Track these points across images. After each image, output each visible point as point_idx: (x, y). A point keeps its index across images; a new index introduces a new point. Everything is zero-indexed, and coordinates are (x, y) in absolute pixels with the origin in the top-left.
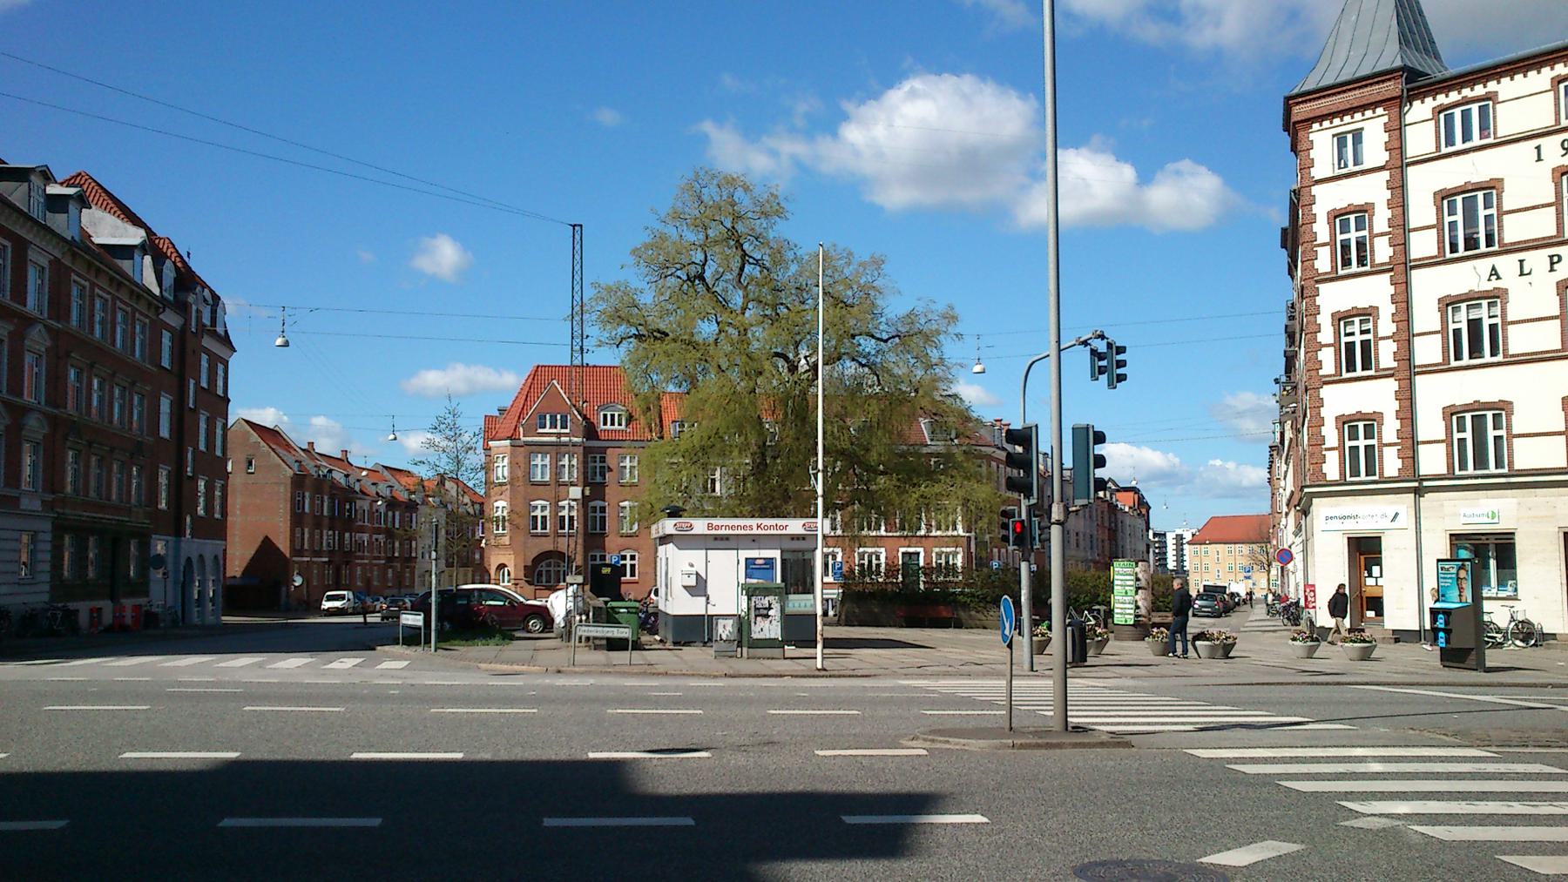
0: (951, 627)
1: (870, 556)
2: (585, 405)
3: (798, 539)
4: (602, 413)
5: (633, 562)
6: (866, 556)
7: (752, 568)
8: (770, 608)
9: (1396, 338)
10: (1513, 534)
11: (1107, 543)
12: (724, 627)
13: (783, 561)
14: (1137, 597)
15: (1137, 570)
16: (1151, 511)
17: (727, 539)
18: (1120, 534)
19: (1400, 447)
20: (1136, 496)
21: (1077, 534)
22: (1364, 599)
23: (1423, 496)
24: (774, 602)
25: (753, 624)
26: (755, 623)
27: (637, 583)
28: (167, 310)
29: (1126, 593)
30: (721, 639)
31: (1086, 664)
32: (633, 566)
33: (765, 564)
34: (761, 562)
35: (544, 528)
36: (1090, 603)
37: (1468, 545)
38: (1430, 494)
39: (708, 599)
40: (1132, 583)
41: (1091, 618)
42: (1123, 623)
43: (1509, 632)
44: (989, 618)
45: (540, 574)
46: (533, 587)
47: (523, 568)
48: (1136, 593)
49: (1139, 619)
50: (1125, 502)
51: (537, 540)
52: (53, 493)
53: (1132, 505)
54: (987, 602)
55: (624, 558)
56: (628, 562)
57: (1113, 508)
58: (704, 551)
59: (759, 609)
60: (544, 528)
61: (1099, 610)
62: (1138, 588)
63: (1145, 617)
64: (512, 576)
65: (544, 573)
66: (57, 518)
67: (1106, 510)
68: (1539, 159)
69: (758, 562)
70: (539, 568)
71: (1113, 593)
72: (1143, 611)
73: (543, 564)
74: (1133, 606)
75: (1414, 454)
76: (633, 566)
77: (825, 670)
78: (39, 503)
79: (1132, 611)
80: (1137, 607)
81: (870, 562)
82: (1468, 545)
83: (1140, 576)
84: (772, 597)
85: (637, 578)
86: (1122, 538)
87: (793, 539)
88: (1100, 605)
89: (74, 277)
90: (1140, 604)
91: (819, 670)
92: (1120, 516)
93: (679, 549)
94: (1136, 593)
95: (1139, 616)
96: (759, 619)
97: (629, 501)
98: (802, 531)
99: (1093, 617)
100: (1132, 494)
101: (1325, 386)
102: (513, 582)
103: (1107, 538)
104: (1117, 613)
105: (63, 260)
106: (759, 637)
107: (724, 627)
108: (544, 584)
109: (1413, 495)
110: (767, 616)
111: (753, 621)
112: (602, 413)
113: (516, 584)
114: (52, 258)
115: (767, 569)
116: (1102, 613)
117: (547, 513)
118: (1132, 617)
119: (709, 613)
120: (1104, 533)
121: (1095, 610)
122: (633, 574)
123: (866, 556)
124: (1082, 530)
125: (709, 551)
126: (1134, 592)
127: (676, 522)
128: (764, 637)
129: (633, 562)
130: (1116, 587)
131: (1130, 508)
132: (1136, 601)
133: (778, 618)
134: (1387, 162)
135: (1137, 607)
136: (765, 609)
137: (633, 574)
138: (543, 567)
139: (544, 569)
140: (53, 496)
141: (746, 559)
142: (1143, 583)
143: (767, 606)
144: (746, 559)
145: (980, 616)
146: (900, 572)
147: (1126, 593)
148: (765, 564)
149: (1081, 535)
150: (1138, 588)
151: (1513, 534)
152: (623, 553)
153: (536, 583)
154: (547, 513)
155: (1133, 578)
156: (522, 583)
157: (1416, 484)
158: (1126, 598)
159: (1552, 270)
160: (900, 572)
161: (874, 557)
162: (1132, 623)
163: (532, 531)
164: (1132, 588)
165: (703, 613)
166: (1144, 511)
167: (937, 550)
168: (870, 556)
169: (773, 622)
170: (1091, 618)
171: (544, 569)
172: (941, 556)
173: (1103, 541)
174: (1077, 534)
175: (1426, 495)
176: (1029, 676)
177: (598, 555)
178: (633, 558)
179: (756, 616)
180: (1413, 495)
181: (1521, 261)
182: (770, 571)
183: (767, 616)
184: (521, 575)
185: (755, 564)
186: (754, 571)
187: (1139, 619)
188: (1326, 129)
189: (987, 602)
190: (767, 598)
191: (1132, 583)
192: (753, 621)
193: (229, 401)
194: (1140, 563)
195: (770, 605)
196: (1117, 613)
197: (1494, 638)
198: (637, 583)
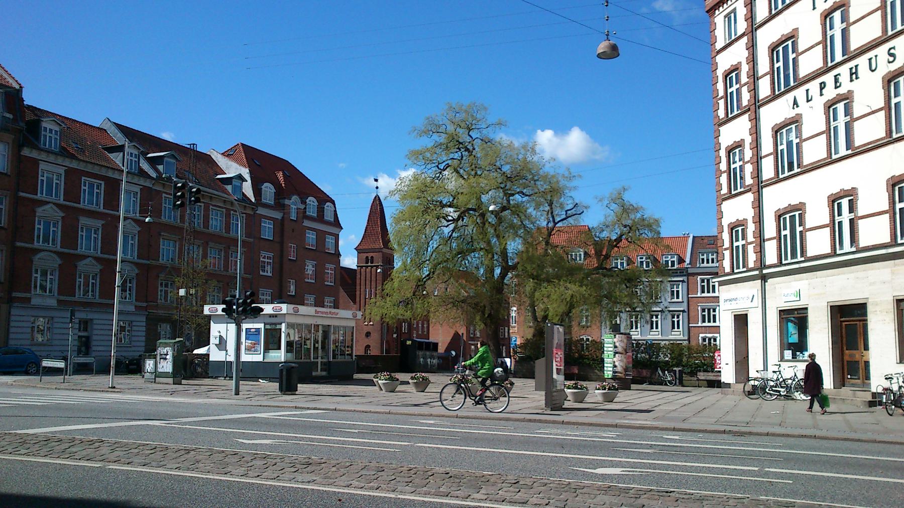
0: (715, 387)
1: (710, 339)
3: (273, 317)
6: (707, 340)
7: (249, 334)
8: (167, 354)
9: (752, 162)
10: (806, 309)
12: (149, 364)
13: (266, 330)
14: (615, 359)
15: (615, 340)
17: (276, 316)
19: (754, 245)
22: (845, 363)
23: (767, 282)
24: (169, 351)
25: (158, 363)
26: (160, 363)
28: (259, 207)
30: (148, 372)
31: (297, 393)
33: (255, 332)
34: (254, 330)
37: (792, 319)
38: (770, 279)
39: (227, 351)
40: (611, 349)
43: (793, 386)
49: (616, 374)
52: (147, 302)
58: (226, 324)
59: (162, 355)
62: (616, 353)
66: (148, 315)
68: (814, 8)
69: (252, 330)
72: (619, 369)
74: (612, 365)
75: (761, 249)
77: (114, 388)
78: (134, 307)
79: (611, 369)
80: (615, 366)
81: (710, 343)
82: (792, 319)
83: (617, 344)
84: (168, 348)
87: (270, 317)
89: (164, 195)
91: (109, 387)
93: (214, 323)
94: (614, 355)
95: (616, 372)
96: (162, 360)
98: (272, 312)
101: (724, 203)
105: (154, 188)
106: (161, 371)
107: (149, 364)
109: (760, 281)
110: (165, 359)
111: (159, 361)
114: (142, 187)
115: (257, 334)
118: (611, 373)
119: (227, 360)
123: (707, 340)
125: (228, 324)
127: (209, 307)
128: (163, 371)
132: (614, 362)
133: (171, 360)
134: (746, 29)
135: (615, 366)
136: (165, 355)
140: (147, 304)
141: (246, 329)
142: (620, 349)
143: (166, 353)
144: (246, 329)
146: (585, 348)
148: (255, 332)
150: (616, 353)
151: (806, 309)
155: (612, 345)
157: (765, 271)
159: (821, 95)
160: (585, 348)
161: (712, 340)
164: (611, 353)
165: (224, 360)
167: (701, 335)
168: (710, 339)
169: (169, 362)
172: (705, 339)
175: (768, 280)
176: (107, 391)
179: (160, 359)
180: (760, 281)
181: (807, 91)
182: (258, 335)
183: (165, 359)
185: (250, 332)
186: (250, 336)
187: (616, 374)
188: (718, 15)
190: (166, 349)
191: (611, 349)
192: (159, 361)
193: (339, 255)
195: (167, 352)
197: (779, 391)
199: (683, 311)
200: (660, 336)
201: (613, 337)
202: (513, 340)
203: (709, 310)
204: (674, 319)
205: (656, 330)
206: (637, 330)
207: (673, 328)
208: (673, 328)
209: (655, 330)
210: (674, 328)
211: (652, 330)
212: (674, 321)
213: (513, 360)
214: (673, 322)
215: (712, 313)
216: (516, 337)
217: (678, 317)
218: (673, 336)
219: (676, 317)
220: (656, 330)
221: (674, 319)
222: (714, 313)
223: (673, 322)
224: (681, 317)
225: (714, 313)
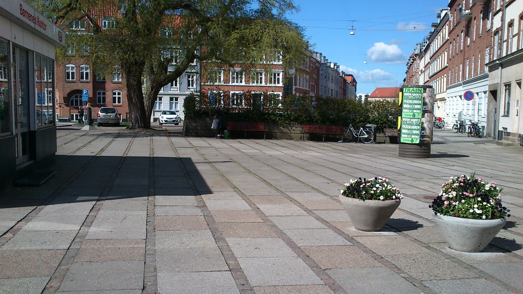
2: (95, 17)
4: (103, 21)
5: (119, 96)
11: (342, 95)
14: (424, 120)
15: (425, 95)
16: (357, 84)
18: (347, 92)
20: (352, 78)
21: (332, 90)
27: (122, 106)
29: (414, 115)
32: (119, 98)
35: (73, 78)
36: (363, 121)
40: (419, 107)
41: (365, 133)
42: (410, 142)
44: (292, 131)
45: (72, 101)
46: (69, 108)
47: (63, 99)
48: (423, 116)
49: (424, 139)
50: (349, 79)
51: (69, 84)
53: (351, 81)
54: (291, 120)
55: (115, 94)
56: (117, 96)
57: (345, 81)
60: (73, 78)
61: (370, 127)
63: (429, 137)
64: (58, 102)
65: (74, 101)
67: (343, 81)
70: (72, 98)
71: (401, 116)
73: (74, 96)
76: (119, 98)
79: (418, 132)
80: (423, 129)
85: (121, 104)
86: (348, 93)
88: (370, 123)
90: (425, 125)
92: (347, 85)
94: (423, 116)
97: (141, 74)
99: (367, 132)
100: (351, 77)
102: (58, 105)
103: (342, 93)
104: (404, 134)
108: (74, 106)
112: (103, 21)
113: (60, 106)
116: (373, 129)
117: (74, 71)
118: (418, 137)
120: (341, 90)
121: (368, 127)
122: (119, 102)
124: (333, 89)
125: (149, 156)
126: (421, 114)
129: (119, 96)
130: (404, 111)
131: (350, 82)
132: (423, 123)
135: (423, 129)
137: (119, 102)
138: (73, 98)
139: (74, 99)
145: (285, 130)
147: (414, 115)
149: (333, 91)
152: (114, 92)
153: (70, 106)
154: (74, 71)
156: (63, 106)
158: (414, 120)
162: (418, 142)
163: (81, 80)
166: (355, 84)
170: (365, 133)
171: (74, 99)
173: (341, 94)
174: (332, 90)
177: (102, 92)
178: (119, 94)
184: (62, 102)
187: (424, 139)
189: (291, 120)
191: (419, 107)
194: (428, 89)
196: (404, 134)
198: (122, 106)
199: (197, 73)
200: (179, 92)
201: (422, 92)
202: (84, 92)
203: (275, 75)
204: (189, 79)
205: (175, 87)
206: (177, 87)
207: (189, 85)
208: (189, 85)
209: (174, 87)
210: (173, 86)
211: (172, 87)
212: (190, 80)
213: (192, 128)
214: (189, 81)
215: (277, 77)
216: (87, 90)
217: (193, 77)
218: (171, 92)
219: (191, 77)
220: (175, 87)
221: (189, 79)
222: (278, 77)
223: (189, 81)
224: (195, 77)
225: (278, 77)
